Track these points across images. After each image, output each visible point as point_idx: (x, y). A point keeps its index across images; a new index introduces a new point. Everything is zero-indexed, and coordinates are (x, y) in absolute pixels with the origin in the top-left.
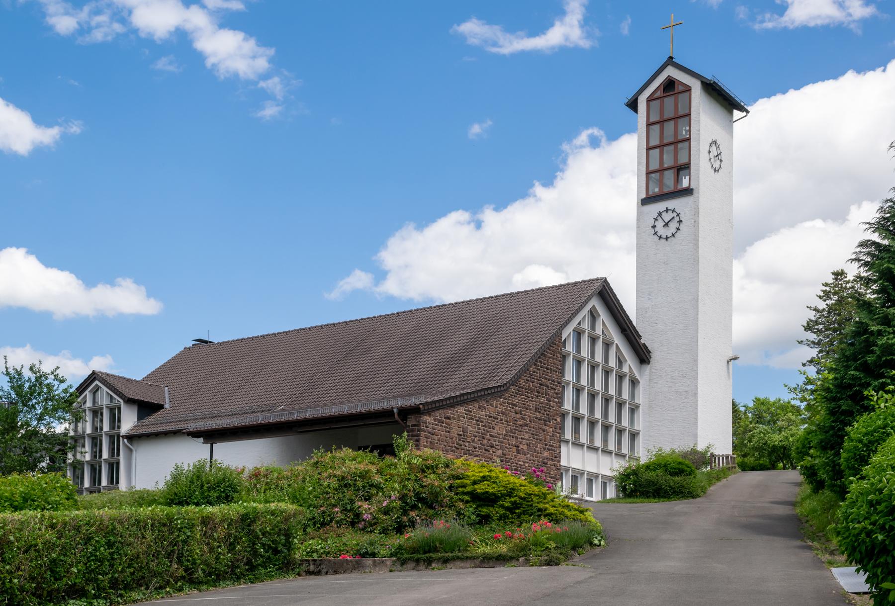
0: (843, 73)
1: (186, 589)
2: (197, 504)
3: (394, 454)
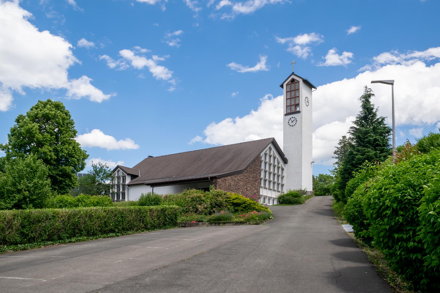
0: (343, 79)
1: (145, 231)
2: (148, 206)
3: (209, 191)
